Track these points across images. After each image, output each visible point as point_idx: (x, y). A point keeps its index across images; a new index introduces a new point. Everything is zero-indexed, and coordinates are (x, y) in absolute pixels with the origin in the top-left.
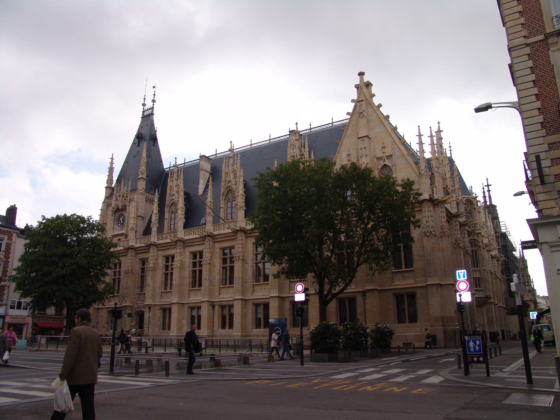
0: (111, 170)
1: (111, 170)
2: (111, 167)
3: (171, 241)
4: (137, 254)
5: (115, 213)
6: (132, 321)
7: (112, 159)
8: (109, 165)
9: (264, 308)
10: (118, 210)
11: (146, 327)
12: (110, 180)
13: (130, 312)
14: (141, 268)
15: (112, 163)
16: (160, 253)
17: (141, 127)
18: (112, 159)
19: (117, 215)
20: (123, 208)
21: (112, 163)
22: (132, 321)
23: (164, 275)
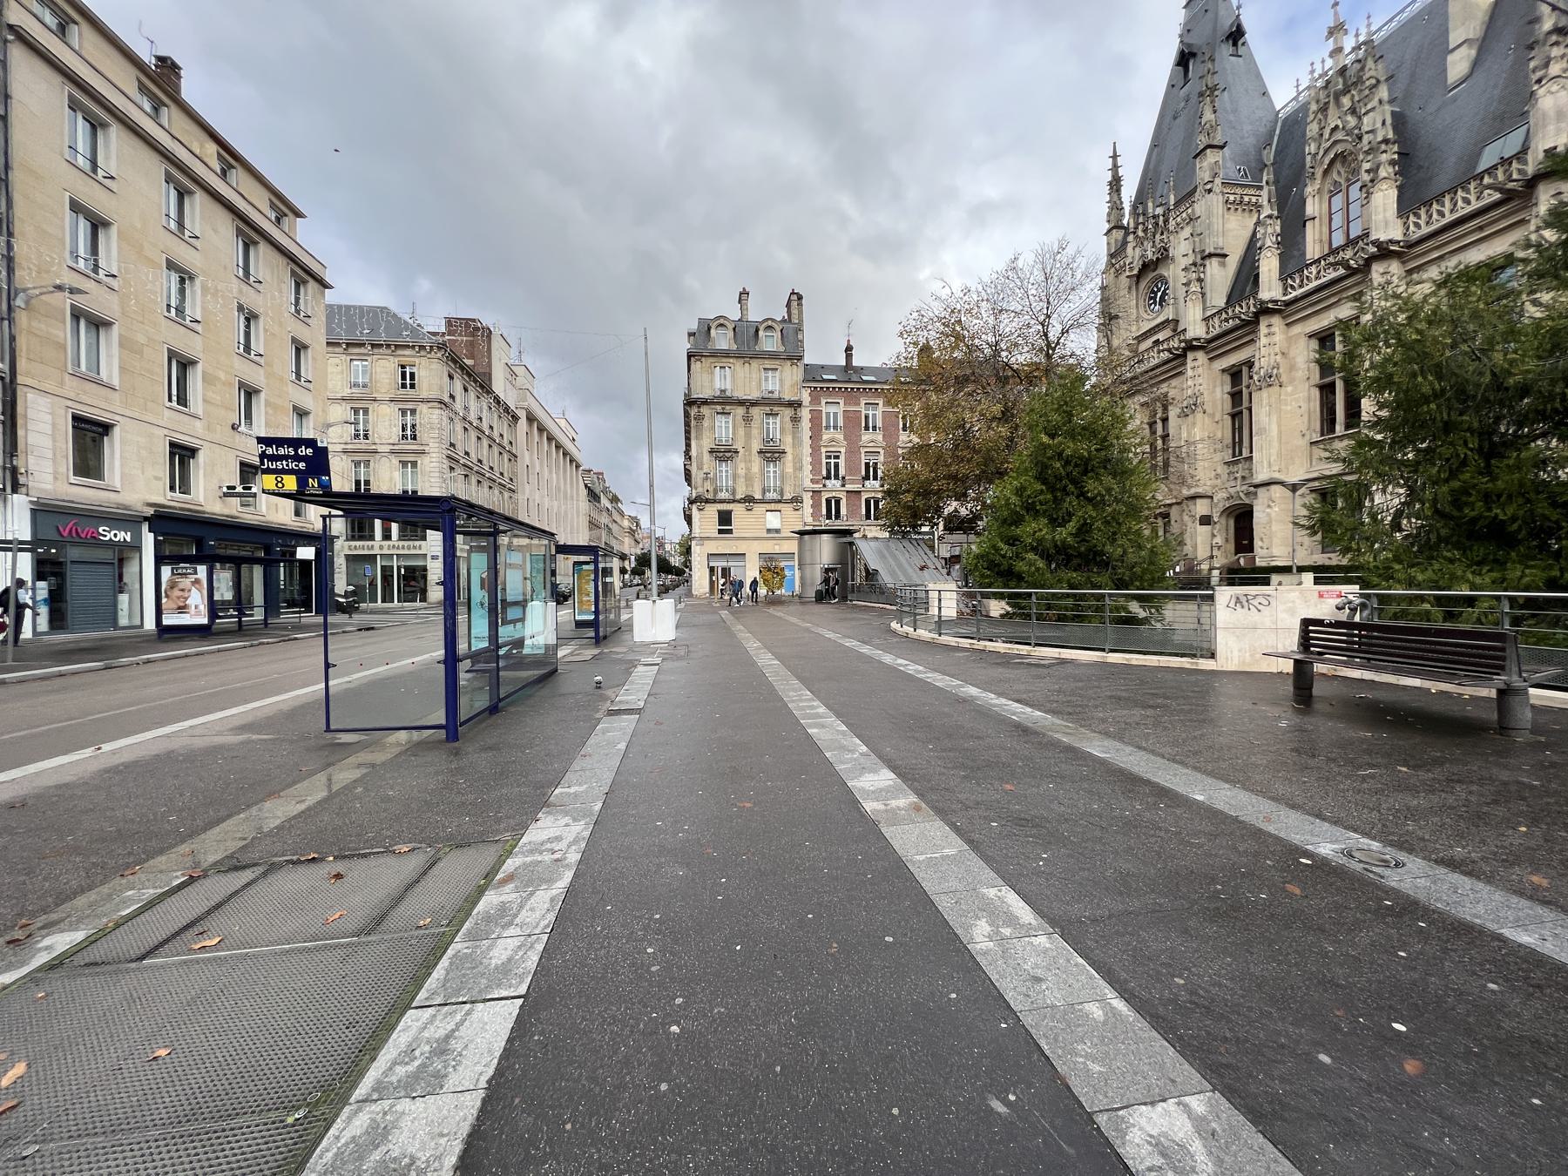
0: (1115, 184)
1: (1115, 184)
2: (1113, 176)
3: (1497, 196)
4: (1410, 272)
5: (1137, 283)
6: (1213, 536)
7: (1115, 157)
8: (1109, 176)
9: (1358, 414)
10: (1147, 267)
11: (1262, 548)
12: (1116, 207)
13: (1205, 512)
14: (1228, 393)
15: (1115, 167)
16: (1297, 329)
17: (1187, 30)
18: (1115, 157)
19: (1143, 284)
20: (1158, 258)
21: (1115, 167)
22: (1213, 536)
23: (1316, 393)
